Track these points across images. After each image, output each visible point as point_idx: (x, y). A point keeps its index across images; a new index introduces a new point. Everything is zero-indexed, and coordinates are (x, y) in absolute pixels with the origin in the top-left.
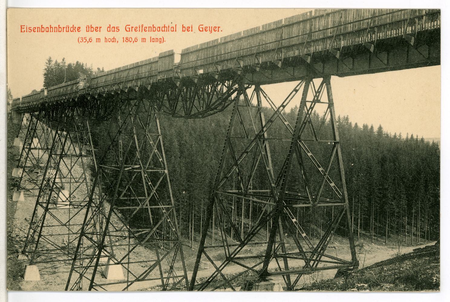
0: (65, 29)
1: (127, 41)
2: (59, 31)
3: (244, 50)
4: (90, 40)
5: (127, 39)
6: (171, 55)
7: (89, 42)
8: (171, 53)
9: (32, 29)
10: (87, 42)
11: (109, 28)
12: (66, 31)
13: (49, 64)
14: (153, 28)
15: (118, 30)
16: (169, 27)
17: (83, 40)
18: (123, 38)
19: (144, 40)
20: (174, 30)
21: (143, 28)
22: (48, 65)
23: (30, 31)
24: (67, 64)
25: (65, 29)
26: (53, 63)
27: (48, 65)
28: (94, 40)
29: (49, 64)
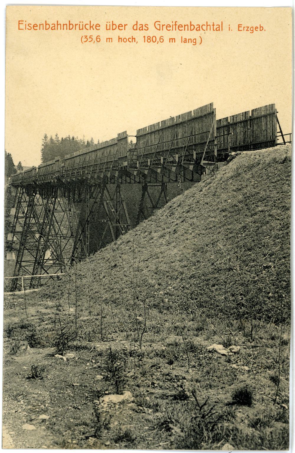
0: (77, 26)
1: (149, 41)
2: (70, 29)
3: (153, 147)
4: (162, 39)
5: (149, 39)
6: (209, 114)
7: (96, 42)
8: (209, 111)
9: (32, 26)
10: (93, 41)
11: (135, 26)
12: (80, 29)
13: (46, 140)
14: (191, 27)
15: (146, 29)
16: (213, 25)
17: (149, 39)
18: (144, 37)
19: (172, 40)
20: (221, 29)
21: (177, 26)
22: (44, 141)
23: (30, 28)
24: (60, 139)
25: (77, 26)
26: (49, 139)
27: (44, 141)
28: (166, 40)
29: (46, 140)
